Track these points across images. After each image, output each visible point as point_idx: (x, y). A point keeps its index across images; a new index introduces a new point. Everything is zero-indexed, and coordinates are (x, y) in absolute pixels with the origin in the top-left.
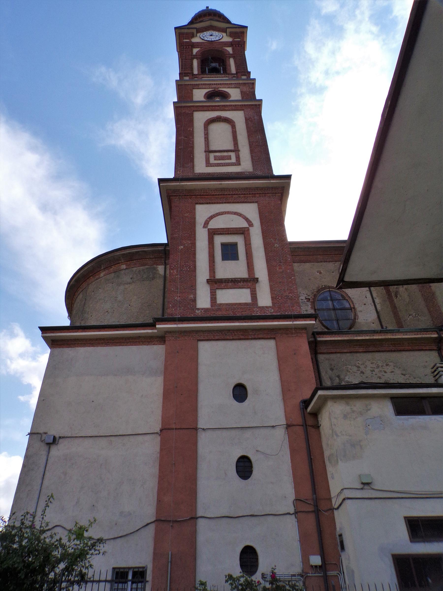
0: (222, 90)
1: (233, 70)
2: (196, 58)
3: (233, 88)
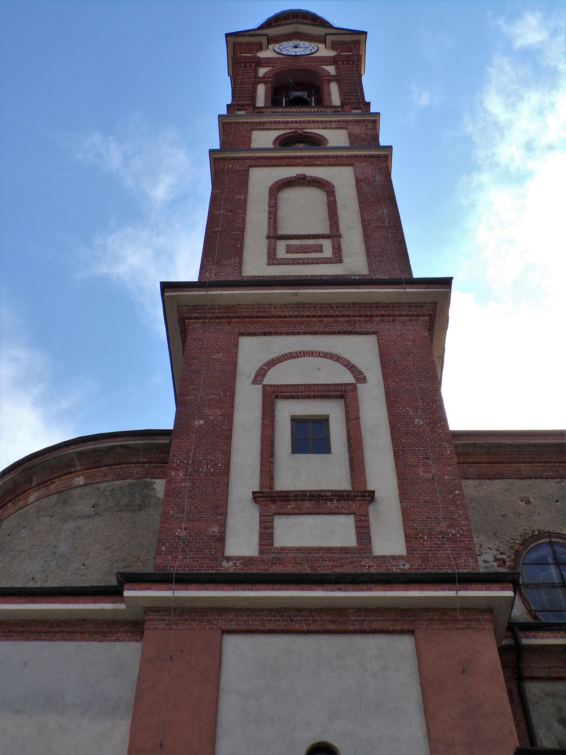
0: (310, 133)
1: (336, 99)
2: (263, 83)
3: (334, 128)
